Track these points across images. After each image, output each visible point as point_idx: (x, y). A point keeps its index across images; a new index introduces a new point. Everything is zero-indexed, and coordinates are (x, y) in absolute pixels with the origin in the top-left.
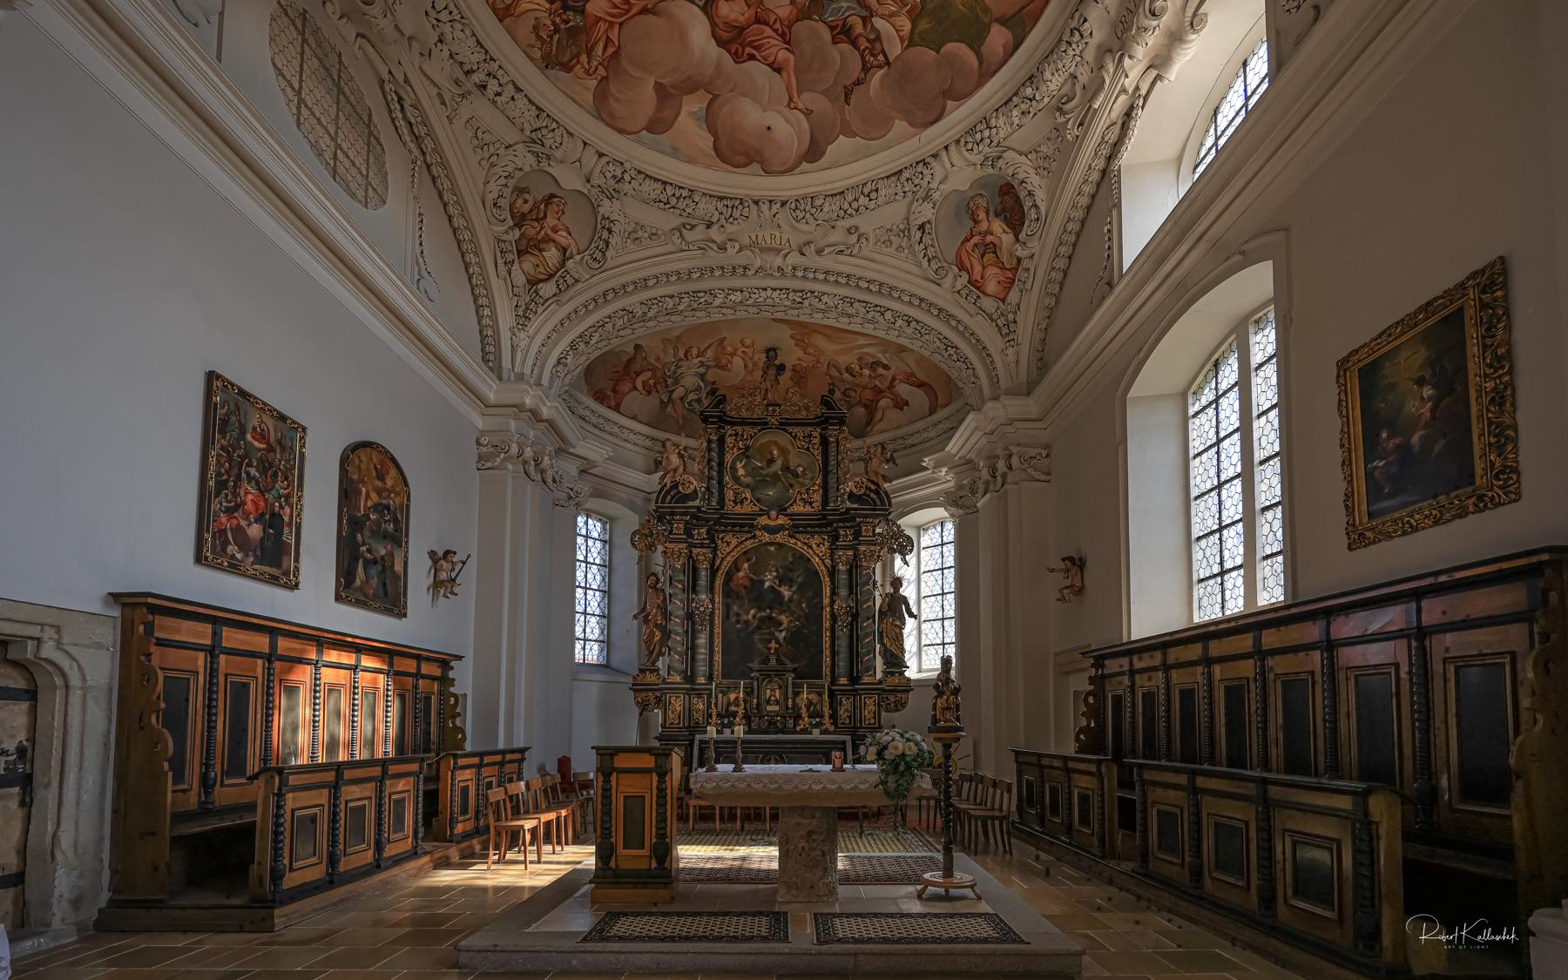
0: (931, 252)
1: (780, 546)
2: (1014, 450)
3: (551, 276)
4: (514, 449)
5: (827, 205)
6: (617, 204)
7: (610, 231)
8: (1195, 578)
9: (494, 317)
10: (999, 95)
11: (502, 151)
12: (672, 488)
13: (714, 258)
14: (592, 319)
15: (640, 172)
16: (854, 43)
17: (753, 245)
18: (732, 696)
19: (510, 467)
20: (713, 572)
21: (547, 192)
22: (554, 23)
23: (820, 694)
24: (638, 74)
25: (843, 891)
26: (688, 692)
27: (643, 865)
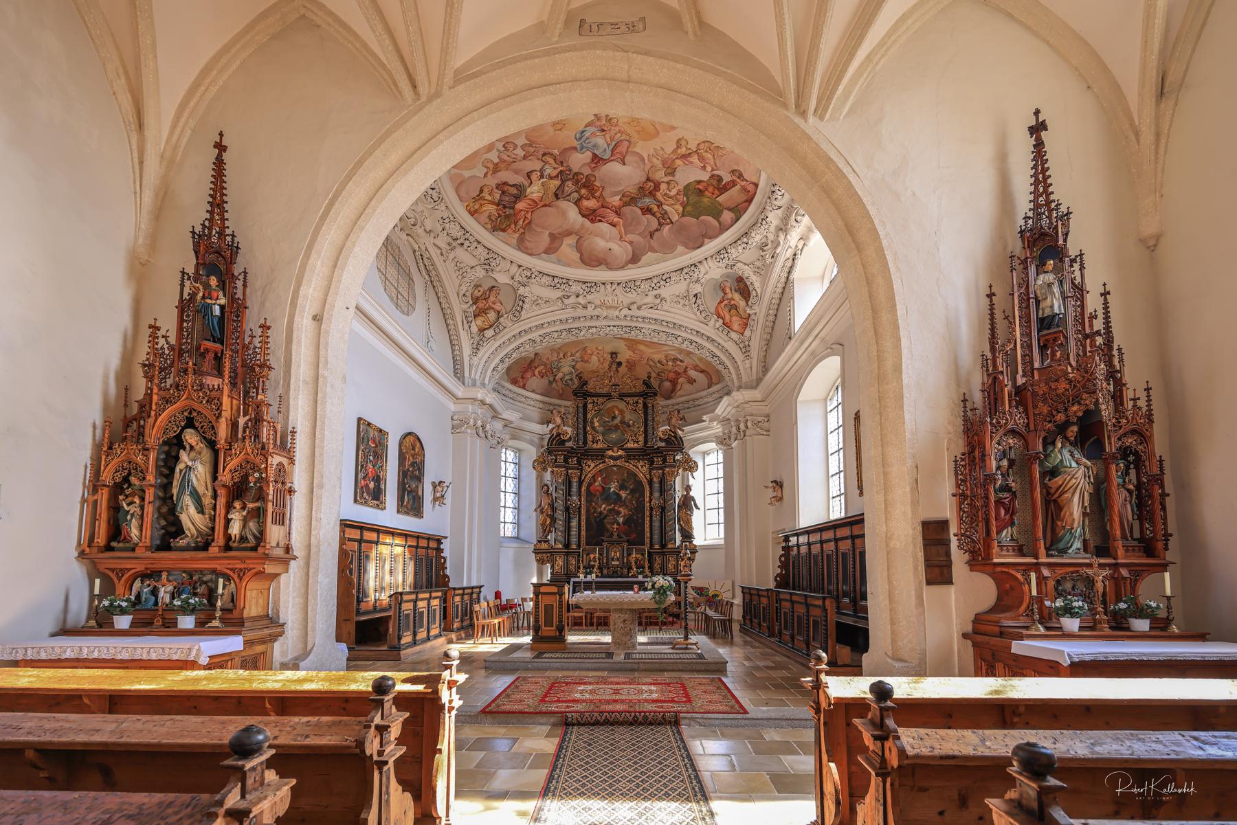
0: (701, 308)
1: (620, 467)
2: (749, 418)
3: (491, 326)
4: (472, 422)
5: (642, 285)
6: (527, 288)
7: (524, 302)
8: (831, 497)
9: (461, 350)
10: (732, 238)
11: (469, 270)
12: (556, 436)
13: (580, 312)
14: (513, 346)
15: (540, 273)
16: (654, 215)
17: (602, 305)
18: (592, 556)
19: (469, 431)
20: (580, 483)
21: (491, 285)
22: (498, 214)
23: (643, 555)
24: (540, 230)
25: (638, 647)
26: (567, 554)
27: (553, 634)
